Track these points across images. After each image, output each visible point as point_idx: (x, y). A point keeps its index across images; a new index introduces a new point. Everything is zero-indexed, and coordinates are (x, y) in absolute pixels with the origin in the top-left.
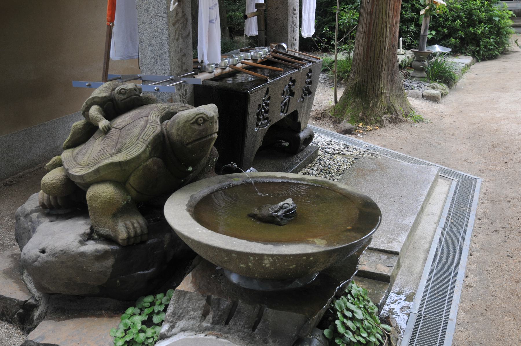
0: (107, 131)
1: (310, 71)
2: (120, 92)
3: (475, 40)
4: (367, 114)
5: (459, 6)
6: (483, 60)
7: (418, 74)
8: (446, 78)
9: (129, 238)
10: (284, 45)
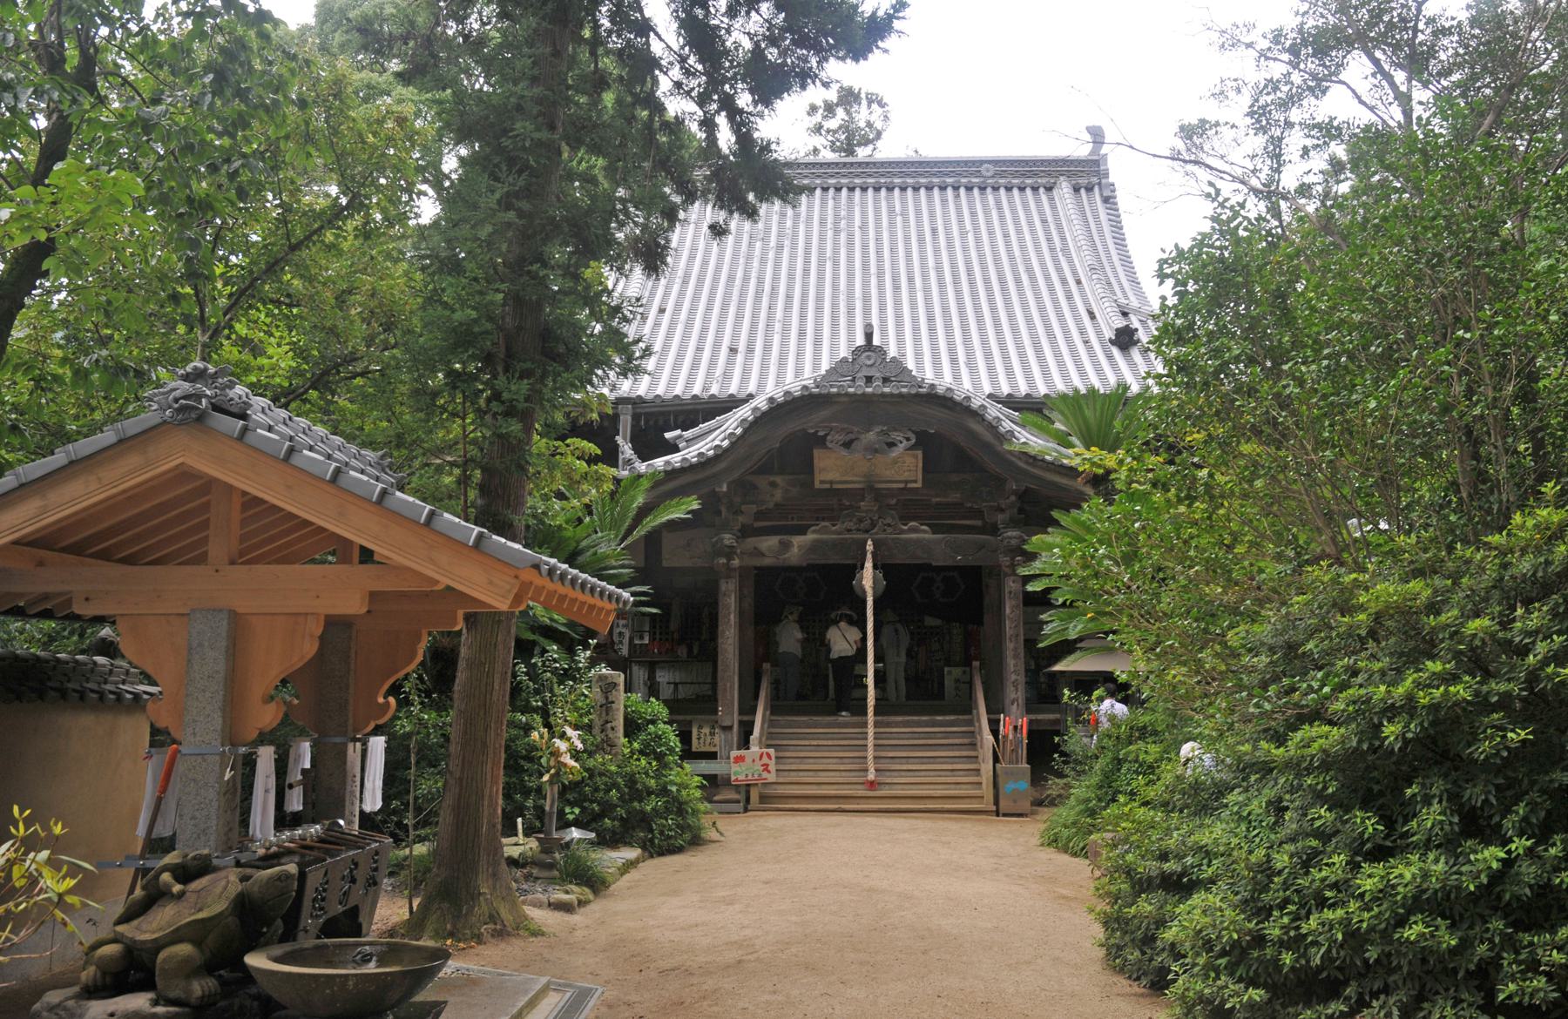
0: (181, 894)
1: (377, 853)
2: (194, 858)
3: (645, 821)
4: (459, 925)
5: (613, 768)
6: (661, 854)
7: (545, 874)
8: (595, 883)
9: (203, 997)
10: (342, 822)
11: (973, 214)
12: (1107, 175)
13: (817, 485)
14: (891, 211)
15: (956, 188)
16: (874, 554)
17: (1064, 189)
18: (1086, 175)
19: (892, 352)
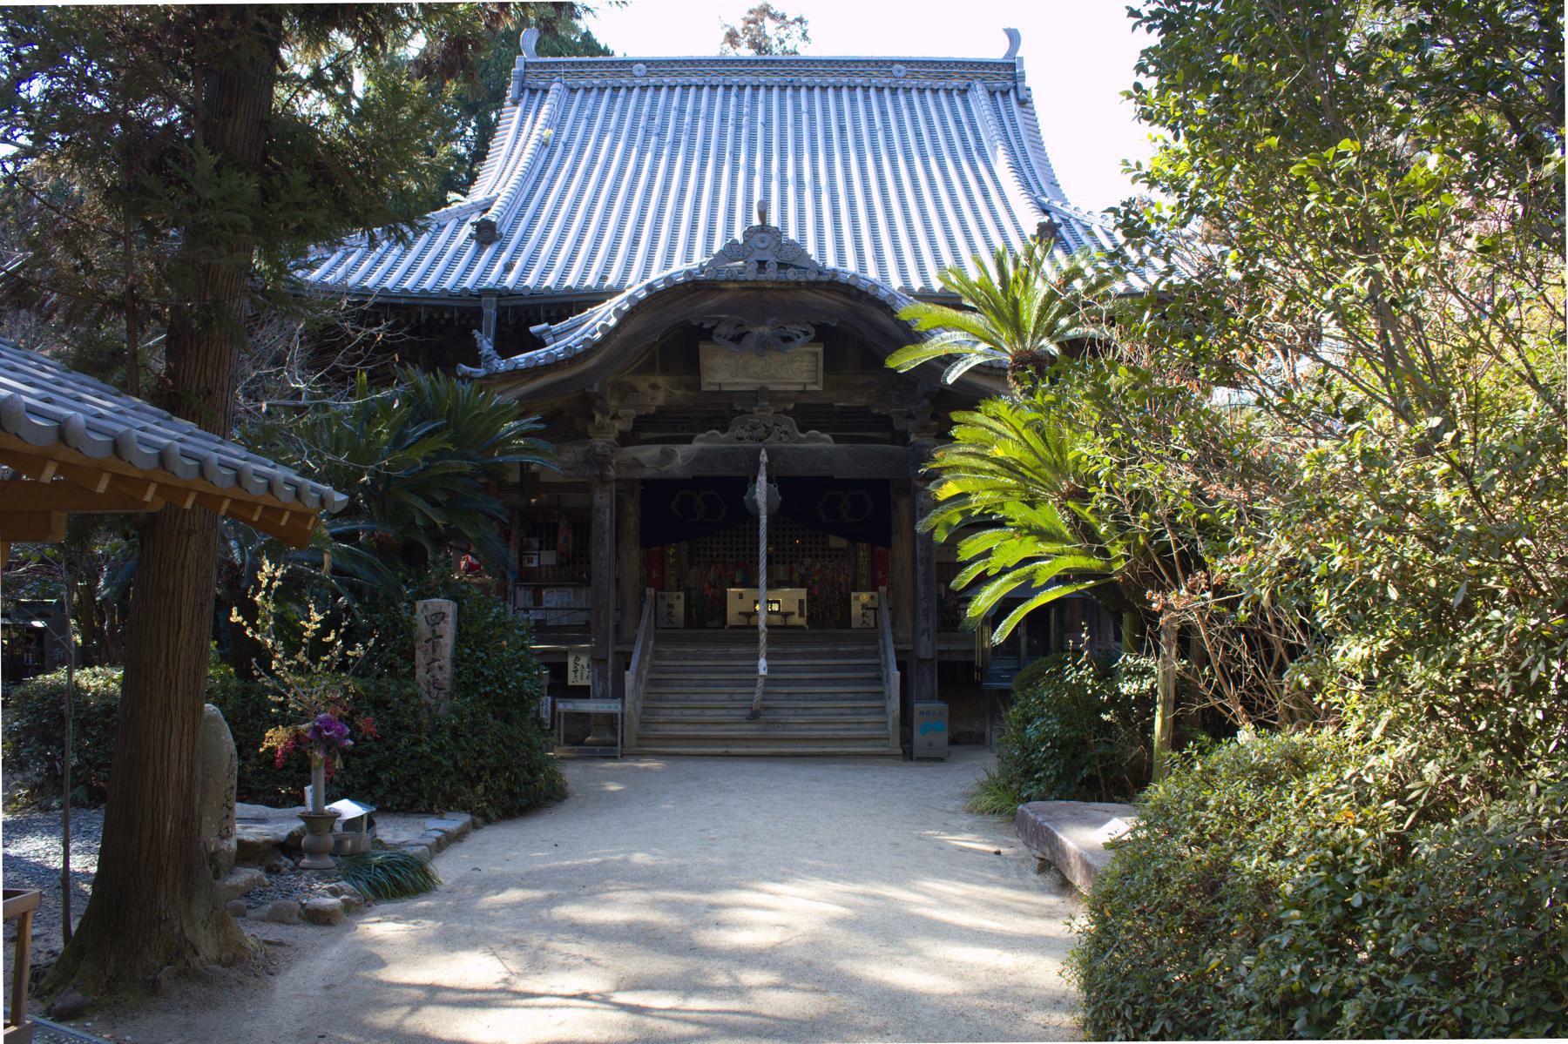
11: (884, 113)
12: (1023, 78)
13: (705, 388)
14: (797, 108)
15: (866, 89)
16: (769, 466)
17: (979, 96)
18: (1003, 80)
19: (792, 234)
